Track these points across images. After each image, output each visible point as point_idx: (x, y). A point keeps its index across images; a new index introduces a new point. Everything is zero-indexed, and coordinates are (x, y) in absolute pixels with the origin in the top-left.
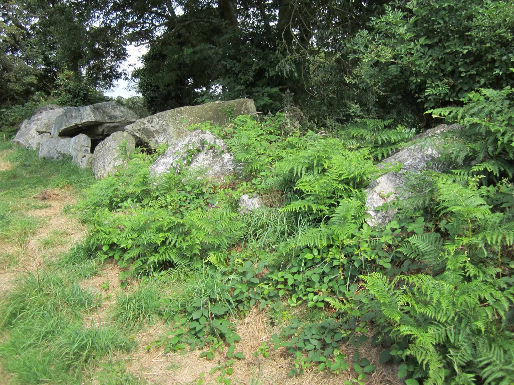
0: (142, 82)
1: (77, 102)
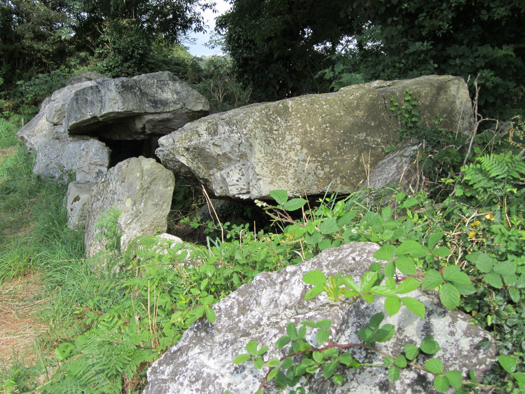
0: (231, 35)
1: (129, 67)
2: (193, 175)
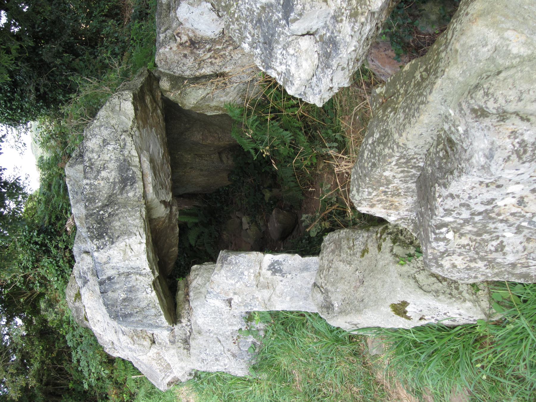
1: (57, 247)
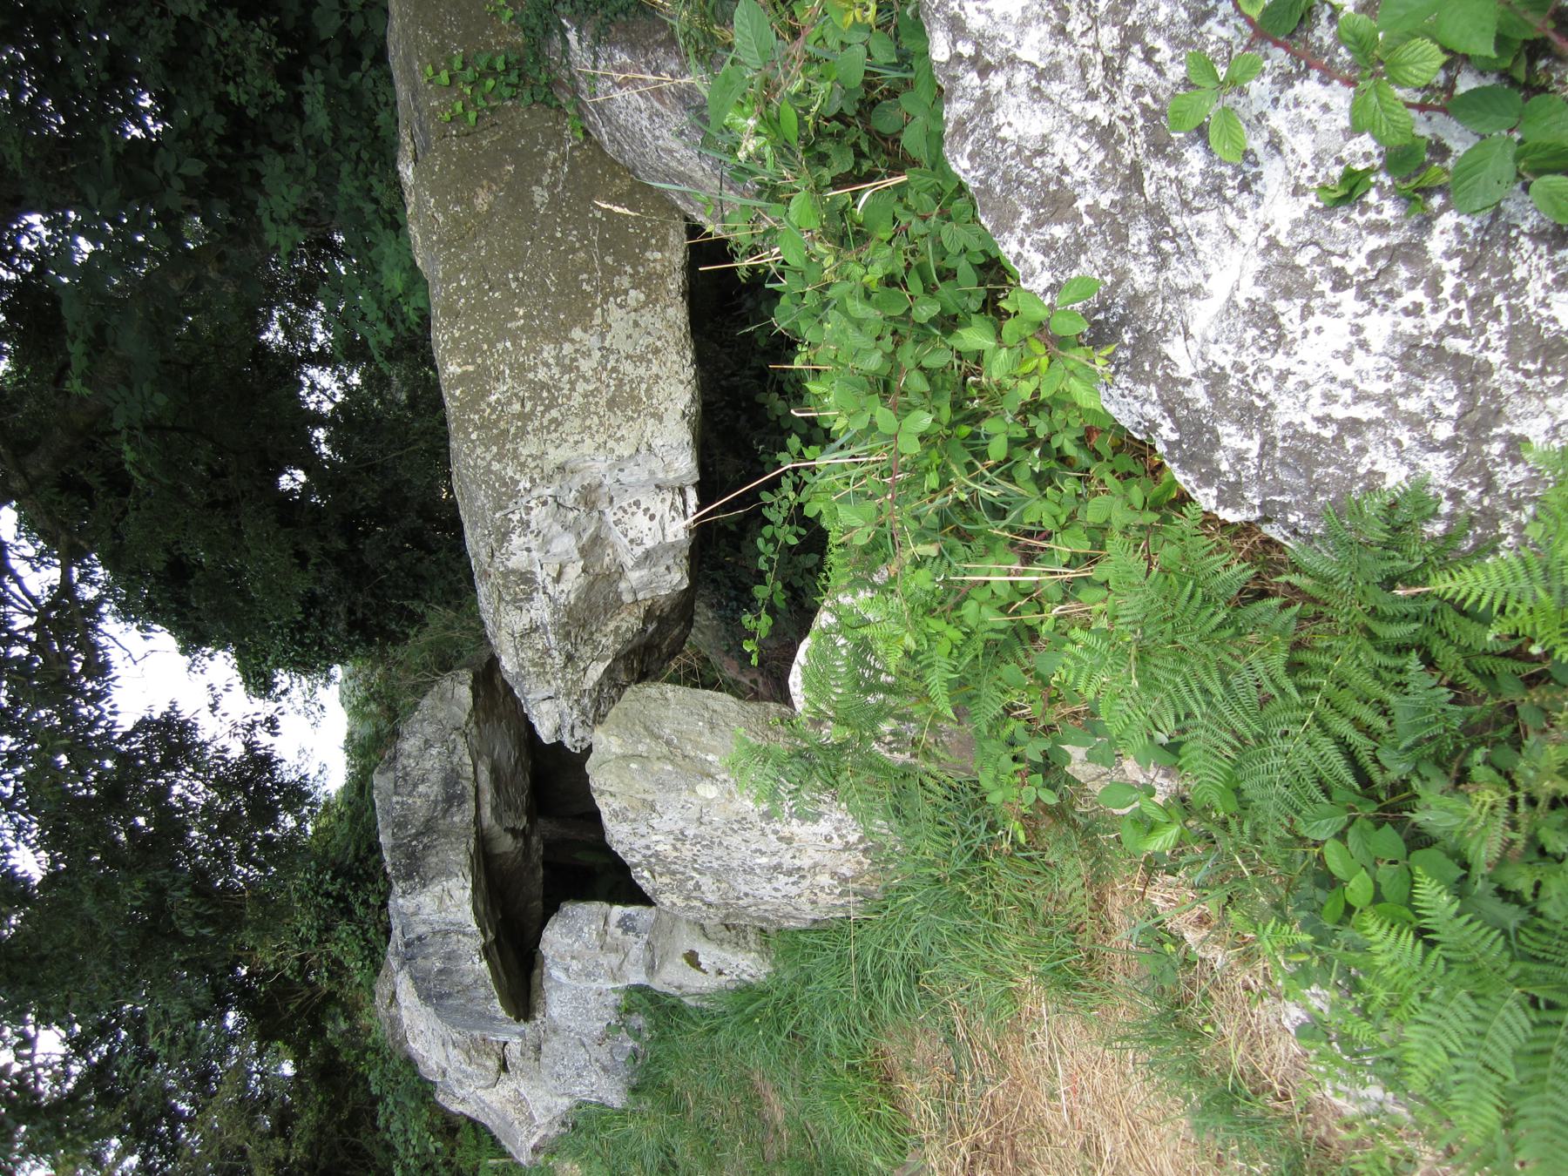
1: (365, 903)
2: (633, 651)
